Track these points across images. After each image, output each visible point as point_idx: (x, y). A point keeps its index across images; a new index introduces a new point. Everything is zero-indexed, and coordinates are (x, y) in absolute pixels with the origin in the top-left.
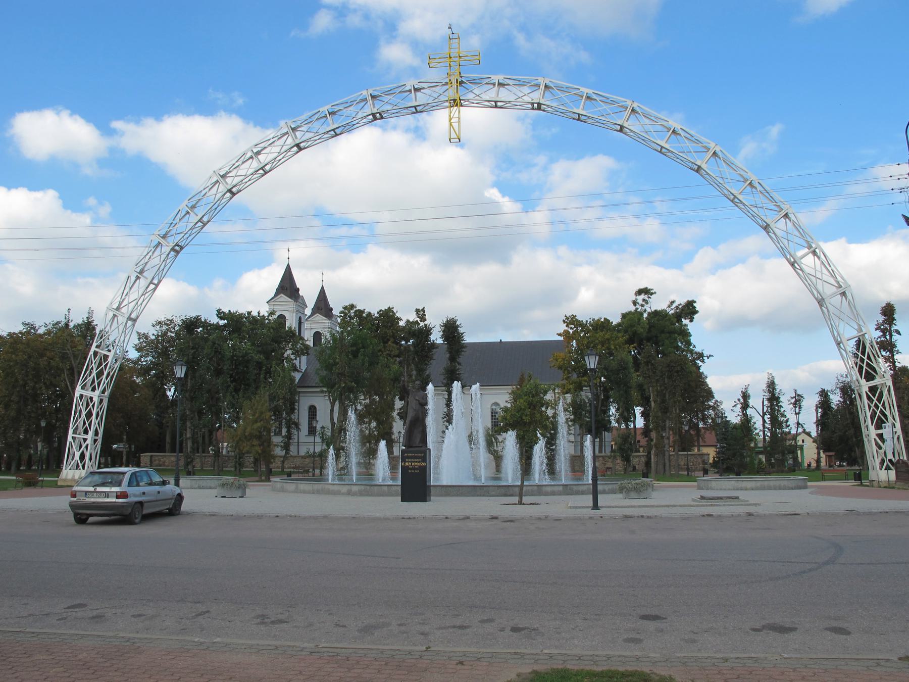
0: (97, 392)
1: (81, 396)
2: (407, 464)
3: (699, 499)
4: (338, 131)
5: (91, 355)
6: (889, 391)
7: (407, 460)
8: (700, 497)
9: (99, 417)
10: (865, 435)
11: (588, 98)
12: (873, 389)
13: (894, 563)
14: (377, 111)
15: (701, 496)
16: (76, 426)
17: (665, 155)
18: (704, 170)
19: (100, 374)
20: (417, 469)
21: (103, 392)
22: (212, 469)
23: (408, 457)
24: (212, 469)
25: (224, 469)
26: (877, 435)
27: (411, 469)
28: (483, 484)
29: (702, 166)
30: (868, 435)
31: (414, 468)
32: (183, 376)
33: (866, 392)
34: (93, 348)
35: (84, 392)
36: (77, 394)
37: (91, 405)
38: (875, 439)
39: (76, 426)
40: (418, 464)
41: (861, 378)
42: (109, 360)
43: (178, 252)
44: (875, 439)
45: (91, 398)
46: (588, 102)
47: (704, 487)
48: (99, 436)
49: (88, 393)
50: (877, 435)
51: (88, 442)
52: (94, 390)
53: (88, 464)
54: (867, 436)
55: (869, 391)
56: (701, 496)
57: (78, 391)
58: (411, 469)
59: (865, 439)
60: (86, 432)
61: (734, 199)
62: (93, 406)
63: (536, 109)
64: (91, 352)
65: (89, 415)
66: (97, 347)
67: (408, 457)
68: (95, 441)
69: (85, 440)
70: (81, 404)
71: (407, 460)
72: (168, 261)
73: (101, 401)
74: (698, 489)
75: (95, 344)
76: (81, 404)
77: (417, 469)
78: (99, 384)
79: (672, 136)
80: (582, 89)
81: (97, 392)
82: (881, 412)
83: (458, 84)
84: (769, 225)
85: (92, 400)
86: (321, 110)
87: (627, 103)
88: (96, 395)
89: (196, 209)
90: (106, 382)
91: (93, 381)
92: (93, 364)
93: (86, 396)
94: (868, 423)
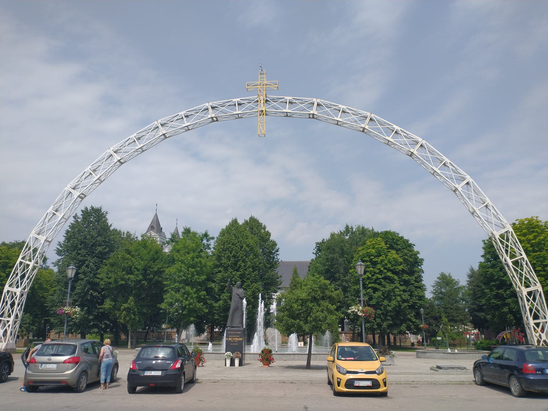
0: (20, 289)
1: (8, 292)
2: (230, 339)
3: (435, 368)
4: (190, 128)
5: (18, 264)
6: (540, 295)
7: (230, 336)
8: (436, 367)
9: (20, 306)
10: (526, 324)
11: (344, 112)
12: (530, 294)
13: (440, 384)
14: (214, 116)
15: (437, 366)
16: (2, 311)
17: (390, 146)
18: (416, 155)
19: (23, 277)
20: (236, 343)
21: (24, 289)
22: (139, 340)
23: (231, 334)
24: (139, 340)
25: (147, 340)
26: (535, 324)
27: (233, 343)
28: (277, 352)
29: (414, 153)
30: (528, 324)
31: (234, 342)
32: (73, 276)
33: (526, 296)
34: (20, 259)
35: (10, 289)
36: (5, 290)
37: (15, 297)
38: (533, 326)
39: (2, 311)
40: (237, 339)
41: (522, 285)
42: (29, 267)
43: (82, 198)
44: (533, 326)
45: (15, 293)
46: (343, 114)
47: (421, 357)
48: (19, 318)
49: (14, 289)
50: (535, 324)
51: (10, 323)
52: (17, 287)
53: (9, 337)
54: (528, 324)
55: (527, 295)
56: (437, 366)
57: (7, 288)
58: (233, 343)
59: (526, 326)
60: (9, 316)
61: (434, 173)
62: (16, 298)
63: (311, 118)
64: (18, 262)
65: (13, 305)
66: (23, 258)
67: (231, 334)
68: (15, 322)
69: (8, 321)
70: (7, 297)
71: (230, 336)
72: (75, 204)
73: (22, 295)
74: (417, 358)
75: (21, 257)
76: (7, 297)
77: (236, 343)
78: (21, 283)
79: (395, 134)
80: (340, 106)
81: (20, 289)
82: (536, 309)
83: (265, 101)
84: (457, 189)
85: (15, 294)
86: (180, 114)
87: (367, 114)
88: (18, 291)
89: (96, 172)
90: (27, 282)
91: (18, 282)
92: (19, 270)
93: (12, 292)
94: (527, 314)
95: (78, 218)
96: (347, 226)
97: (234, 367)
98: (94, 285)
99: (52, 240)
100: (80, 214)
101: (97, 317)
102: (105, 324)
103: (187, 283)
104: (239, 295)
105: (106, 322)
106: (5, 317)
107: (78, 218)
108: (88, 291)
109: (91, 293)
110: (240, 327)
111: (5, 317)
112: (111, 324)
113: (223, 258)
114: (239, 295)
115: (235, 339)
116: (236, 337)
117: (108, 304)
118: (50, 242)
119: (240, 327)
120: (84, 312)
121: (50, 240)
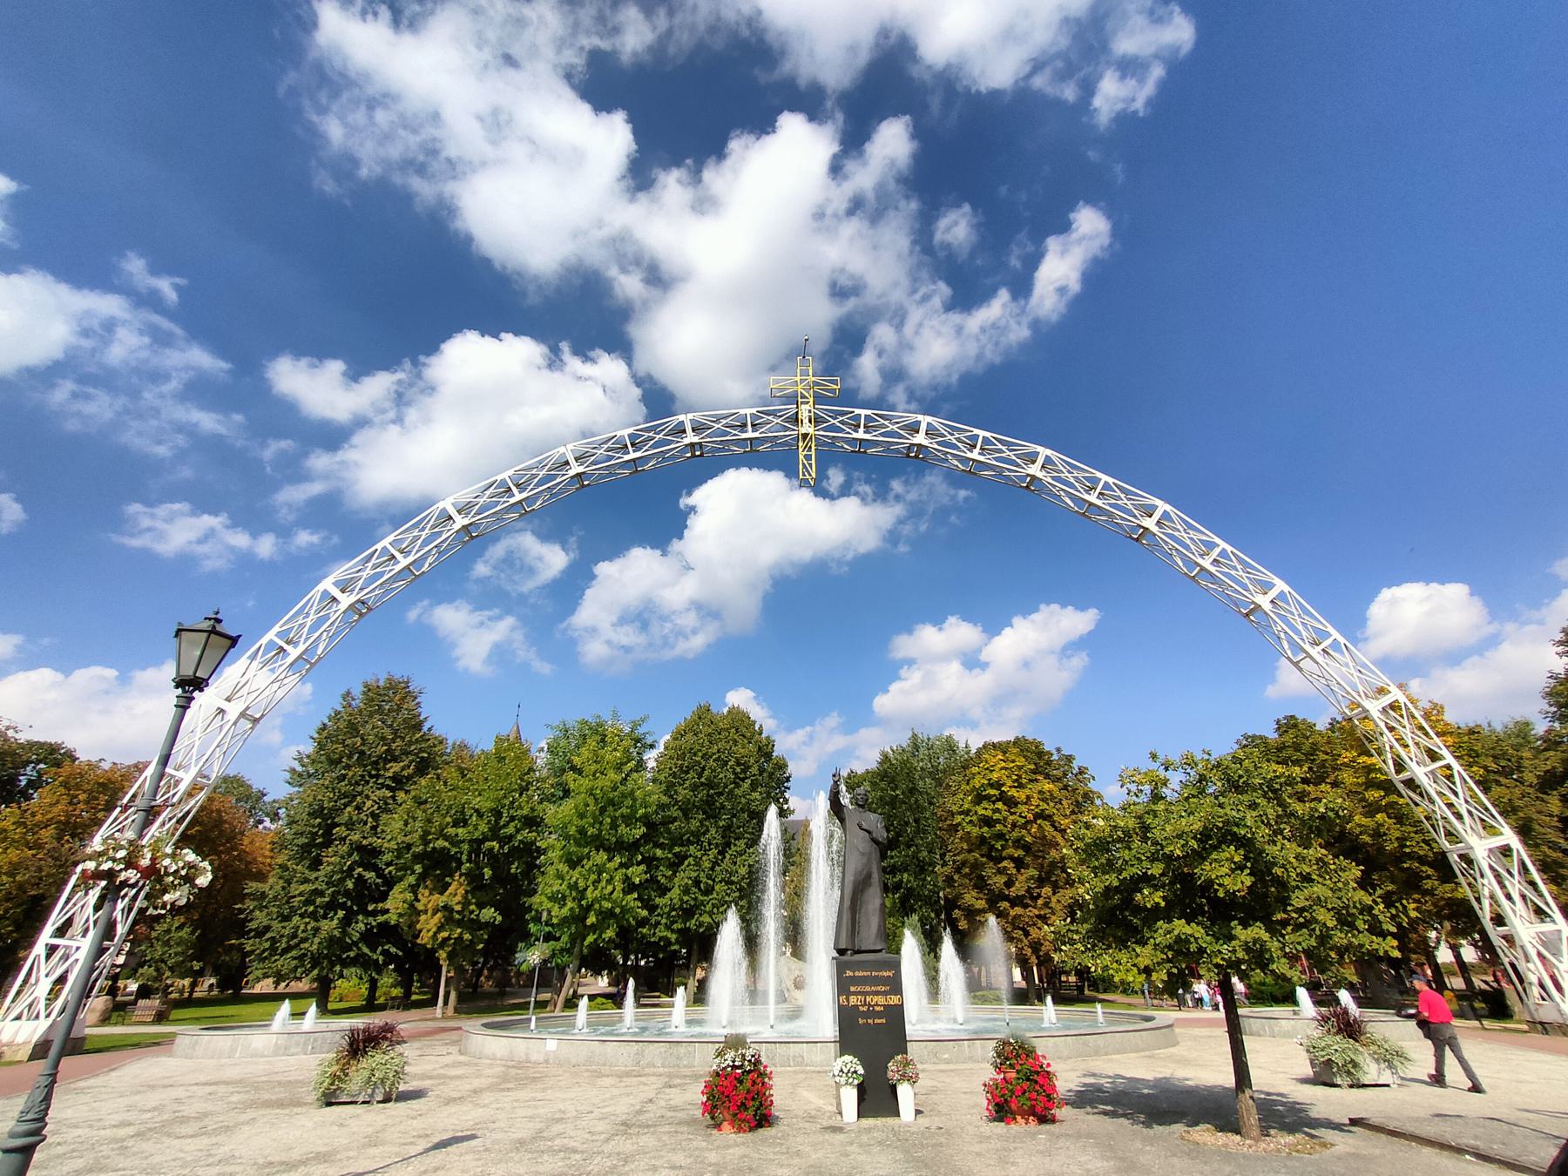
2: (853, 1000)
7: (852, 989)
40: (880, 1000)
58: (866, 1015)
71: (852, 989)
95: (353, 699)
96: (915, 736)
97: (890, 1121)
98: (368, 855)
99: (263, 716)
100: (358, 691)
101: (369, 937)
102: (385, 953)
103: (599, 843)
104: (869, 832)
105: (386, 947)
106: (71, 939)
107: (353, 699)
108: (351, 869)
109: (359, 874)
110: (880, 951)
111: (73, 936)
112: (861, 1021)
113: (680, 789)
114: (869, 832)
115: (876, 998)
116: (877, 993)
117: (396, 903)
118: (256, 721)
119: (880, 951)
120: (336, 921)
121: (257, 716)
